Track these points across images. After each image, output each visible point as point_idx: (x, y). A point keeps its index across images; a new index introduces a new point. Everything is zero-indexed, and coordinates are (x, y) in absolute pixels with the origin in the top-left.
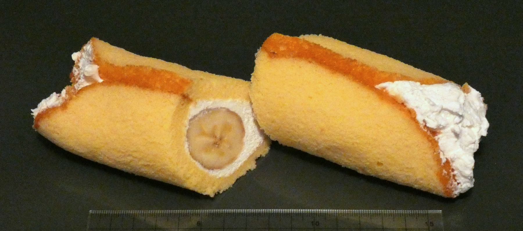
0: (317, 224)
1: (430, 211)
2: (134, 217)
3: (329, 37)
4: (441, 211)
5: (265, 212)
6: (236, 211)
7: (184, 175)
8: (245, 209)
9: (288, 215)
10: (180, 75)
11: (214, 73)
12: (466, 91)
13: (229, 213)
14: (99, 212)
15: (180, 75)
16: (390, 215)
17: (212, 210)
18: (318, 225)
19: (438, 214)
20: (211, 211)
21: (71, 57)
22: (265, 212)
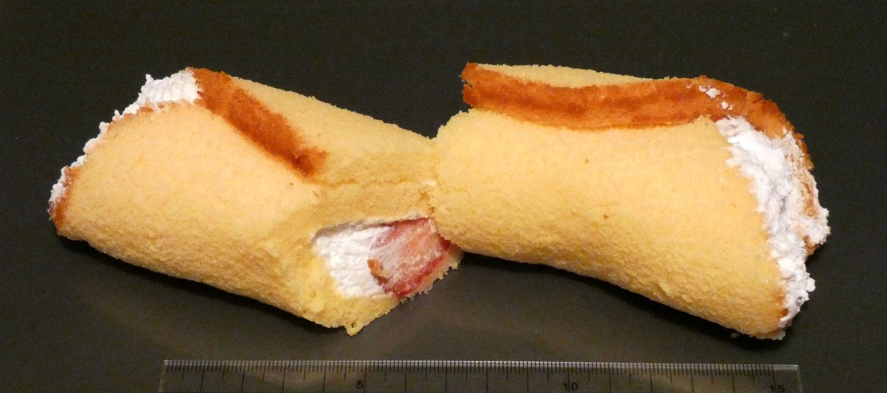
0: (575, 387)
1: (777, 367)
2: (244, 373)
3: (349, 110)
4: (796, 365)
5: (527, 367)
6: (548, 364)
7: (782, 272)
8: (367, 359)
9: (565, 372)
10: (465, 73)
11: (537, 64)
12: (800, 150)
13: (597, 369)
14: (176, 363)
15: (465, 73)
16: (444, 371)
17: (393, 361)
18: (576, 389)
19: (793, 373)
20: (382, 363)
21: (149, 74)
22: (527, 367)
